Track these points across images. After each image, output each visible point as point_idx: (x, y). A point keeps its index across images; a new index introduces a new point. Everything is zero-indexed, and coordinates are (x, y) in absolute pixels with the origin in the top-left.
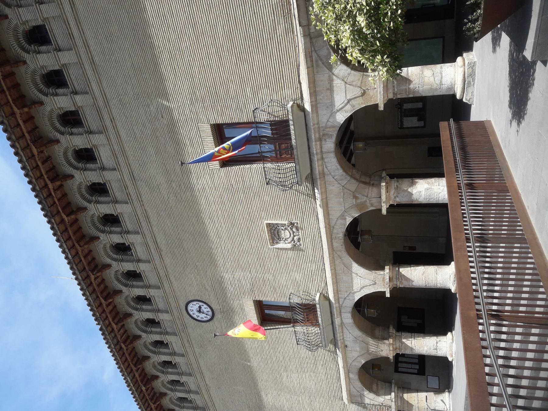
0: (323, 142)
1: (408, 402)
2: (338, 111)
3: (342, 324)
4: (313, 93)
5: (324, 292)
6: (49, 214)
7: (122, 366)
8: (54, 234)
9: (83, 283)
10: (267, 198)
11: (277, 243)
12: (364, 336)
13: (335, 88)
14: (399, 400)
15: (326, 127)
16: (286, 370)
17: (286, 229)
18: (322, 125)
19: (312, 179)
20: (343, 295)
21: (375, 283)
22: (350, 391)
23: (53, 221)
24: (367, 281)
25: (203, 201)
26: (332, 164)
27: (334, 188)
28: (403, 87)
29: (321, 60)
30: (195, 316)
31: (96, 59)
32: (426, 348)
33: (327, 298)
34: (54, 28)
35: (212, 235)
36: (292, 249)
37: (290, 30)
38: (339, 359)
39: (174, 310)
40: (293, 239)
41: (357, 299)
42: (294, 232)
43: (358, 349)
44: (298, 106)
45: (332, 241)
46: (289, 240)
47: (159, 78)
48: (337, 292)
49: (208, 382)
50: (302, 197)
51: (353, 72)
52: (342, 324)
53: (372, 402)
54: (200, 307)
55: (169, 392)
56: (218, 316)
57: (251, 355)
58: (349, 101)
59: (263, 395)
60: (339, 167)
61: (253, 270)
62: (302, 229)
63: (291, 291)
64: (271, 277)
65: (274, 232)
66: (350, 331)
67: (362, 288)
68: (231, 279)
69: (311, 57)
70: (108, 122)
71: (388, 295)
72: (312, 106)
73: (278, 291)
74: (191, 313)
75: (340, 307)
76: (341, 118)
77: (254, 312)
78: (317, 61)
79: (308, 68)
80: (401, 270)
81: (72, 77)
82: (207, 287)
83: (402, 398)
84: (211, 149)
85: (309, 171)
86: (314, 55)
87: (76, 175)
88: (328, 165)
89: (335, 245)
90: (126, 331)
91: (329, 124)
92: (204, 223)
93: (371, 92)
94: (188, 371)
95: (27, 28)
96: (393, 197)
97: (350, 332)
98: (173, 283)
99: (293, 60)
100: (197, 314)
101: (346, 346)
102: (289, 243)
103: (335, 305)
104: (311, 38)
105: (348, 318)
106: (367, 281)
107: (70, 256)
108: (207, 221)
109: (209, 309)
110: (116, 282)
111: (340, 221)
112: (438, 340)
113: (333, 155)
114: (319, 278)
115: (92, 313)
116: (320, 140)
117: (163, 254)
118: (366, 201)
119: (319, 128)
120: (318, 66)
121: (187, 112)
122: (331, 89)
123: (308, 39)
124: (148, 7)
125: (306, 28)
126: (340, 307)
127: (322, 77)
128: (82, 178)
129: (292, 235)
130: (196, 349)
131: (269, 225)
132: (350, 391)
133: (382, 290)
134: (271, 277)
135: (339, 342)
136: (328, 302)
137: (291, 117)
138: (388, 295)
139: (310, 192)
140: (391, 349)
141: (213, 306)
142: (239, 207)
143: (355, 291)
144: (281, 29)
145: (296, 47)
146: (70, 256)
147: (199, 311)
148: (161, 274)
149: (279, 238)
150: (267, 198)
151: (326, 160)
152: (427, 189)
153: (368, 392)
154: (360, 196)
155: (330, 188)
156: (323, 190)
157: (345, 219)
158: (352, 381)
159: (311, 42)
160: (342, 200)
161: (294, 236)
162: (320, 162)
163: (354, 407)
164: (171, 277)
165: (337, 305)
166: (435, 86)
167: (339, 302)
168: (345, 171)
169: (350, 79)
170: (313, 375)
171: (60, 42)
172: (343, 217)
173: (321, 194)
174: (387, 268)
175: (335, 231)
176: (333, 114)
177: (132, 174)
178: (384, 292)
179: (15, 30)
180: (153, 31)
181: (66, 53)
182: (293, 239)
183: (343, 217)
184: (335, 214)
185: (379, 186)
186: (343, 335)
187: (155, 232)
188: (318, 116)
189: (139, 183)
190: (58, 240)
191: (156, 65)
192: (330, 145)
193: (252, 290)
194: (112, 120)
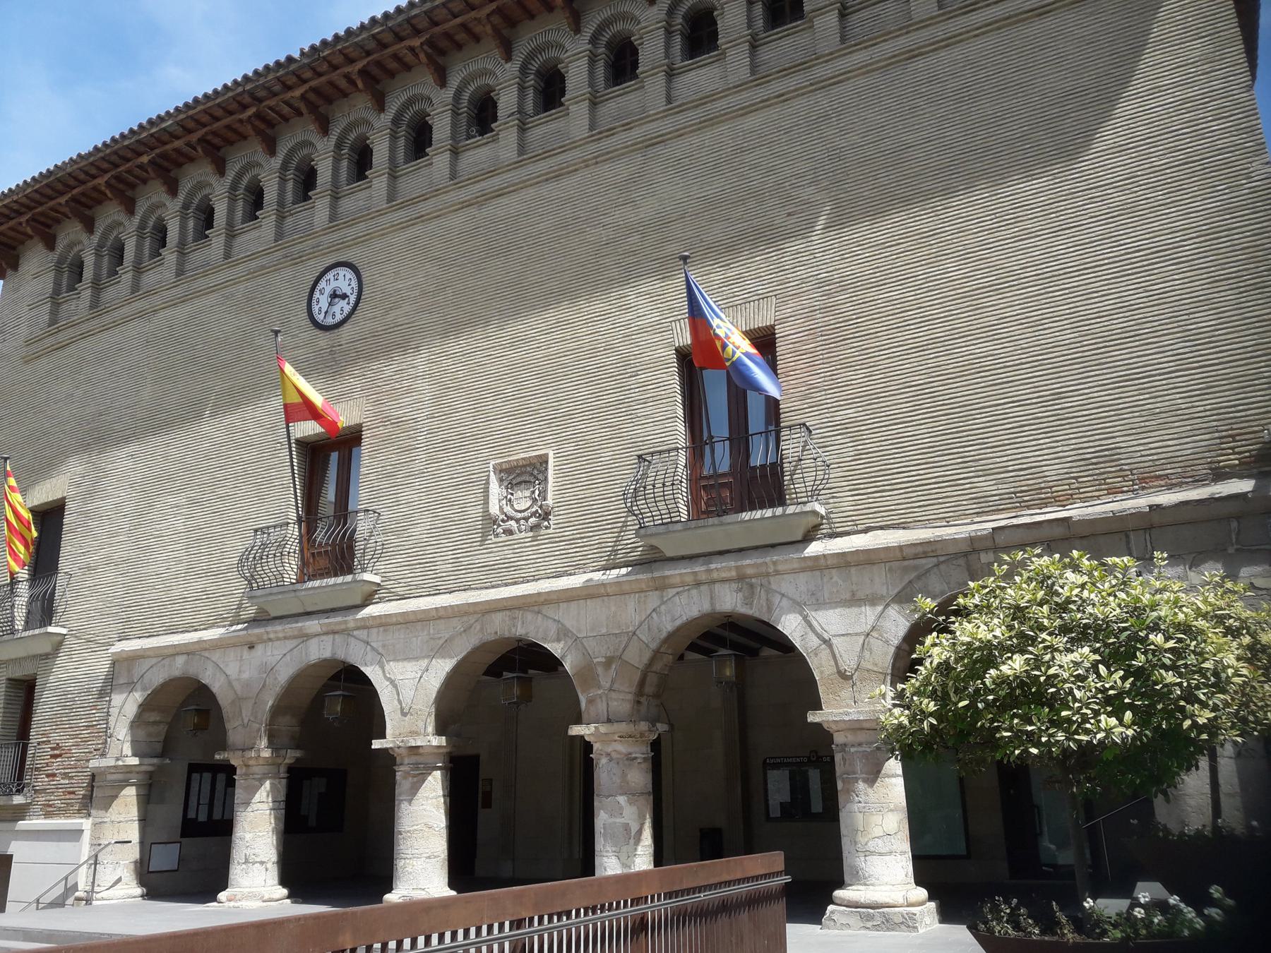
0: (734, 586)
2: (805, 618)
3: (305, 637)
4: (845, 561)
7: (200, 108)
9: (400, 19)
10: (606, 455)
11: (501, 480)
13: (855, 610)
14: (120, 777)
15: (769, 591)
16: (193, 502)
17: (535, 500)
20: (376, 638)
21: (404, 714)
22: (143, 657)
24: (409, 695)
26: (686, 605)
27: (631, 613)
29: (919, 578)
30: (322, 284)
31: (920, 64)
32: (248, 836)
33: (367, 601)
35: (517, 328)
37: (985, 507)
38: (222, 630)
40: (510, 518)
42: (526, 519)
43: (245, 676)
44: (816, 527)
46: (508, 509)
47: (876, 208)
48: (384, 623)
49: (161, 314)
50: (609, 538)
51: (892, 650)
52: (305, 637)
54: (344, 296)
55: (136, 220)
56: (324, 339)
57: (228, 420)
58: (827, 642)
59: (132, 448)
62: (534, 539)
63: (386, 515)
64: (417, 466)
65: (525, 474)
67: (392, 682)
69: (925, 555)
70: (777, 87)
71: (376, 744)
74: (330, 275)
75: (346, 632)
76: (790, 625)
78: (916, 568)
79: (900, 548)
80: (438, 774)
82: (393, 314)
83: (125, 784)
87: (655, 9)
88: (684, 599)
89: (498, 618)
93: (846, 693)
94: (188, 267)
96: (609, 750)
99: (918, 513)
100: (328, 290)
101: (251, 647)
102: (501, 508)
105: (320, 650)
106: (409, 695)
109: (339, 317)
111: (553, 629)
112: (269, 865)
113: (706, 607)
115: (330, 39)
116: (741, 578)
117: (473, 210)
119: (768, 575)
120: (906, 570)
121: (802, 272)
122: (854, 601)
123: (965, 548)
124: (1036, 184)
125: (989, 544)
126: (346, 632)
127: (879, 581)
129: (519, 515)
130: (242, 287)
131: (544, 460)
132: (143, 657)
133: (389, 731)
134: (417, 466)
136: (358, 602)
138: (376, 744)
141: (347, 326)
142: (584, 392)
143: (387, 667)
144: (986, 486)
148: (421, 205)
149: (512, 486)
150: (606, 455)
151: (694, 592)
153: (140, 700)
154: (612, 672)
155: (631, 602)
156: (626, 588)
157: (558, 640)
158: (166, 662)
159: (956, 556)
160: (604, 631)
161: (517, 521)
162: (689, 579)
165: (351, 625)
166: (861, 839)
167: (358, 628)
168: (671, 636)
169: (875, 643)
173: (617, 583)
174: (442, 741)
175: (529, 616)
176: (798, 606)
177: (660, 140)
180: (982, 195)
182: (510, 518)
184: (571, 617)
186: (278, 639)
187: (524, 192)
188: (794, 571)
191: (906, 201)
192: (730, 601)
193: (386, 420)
194: (782, 98)
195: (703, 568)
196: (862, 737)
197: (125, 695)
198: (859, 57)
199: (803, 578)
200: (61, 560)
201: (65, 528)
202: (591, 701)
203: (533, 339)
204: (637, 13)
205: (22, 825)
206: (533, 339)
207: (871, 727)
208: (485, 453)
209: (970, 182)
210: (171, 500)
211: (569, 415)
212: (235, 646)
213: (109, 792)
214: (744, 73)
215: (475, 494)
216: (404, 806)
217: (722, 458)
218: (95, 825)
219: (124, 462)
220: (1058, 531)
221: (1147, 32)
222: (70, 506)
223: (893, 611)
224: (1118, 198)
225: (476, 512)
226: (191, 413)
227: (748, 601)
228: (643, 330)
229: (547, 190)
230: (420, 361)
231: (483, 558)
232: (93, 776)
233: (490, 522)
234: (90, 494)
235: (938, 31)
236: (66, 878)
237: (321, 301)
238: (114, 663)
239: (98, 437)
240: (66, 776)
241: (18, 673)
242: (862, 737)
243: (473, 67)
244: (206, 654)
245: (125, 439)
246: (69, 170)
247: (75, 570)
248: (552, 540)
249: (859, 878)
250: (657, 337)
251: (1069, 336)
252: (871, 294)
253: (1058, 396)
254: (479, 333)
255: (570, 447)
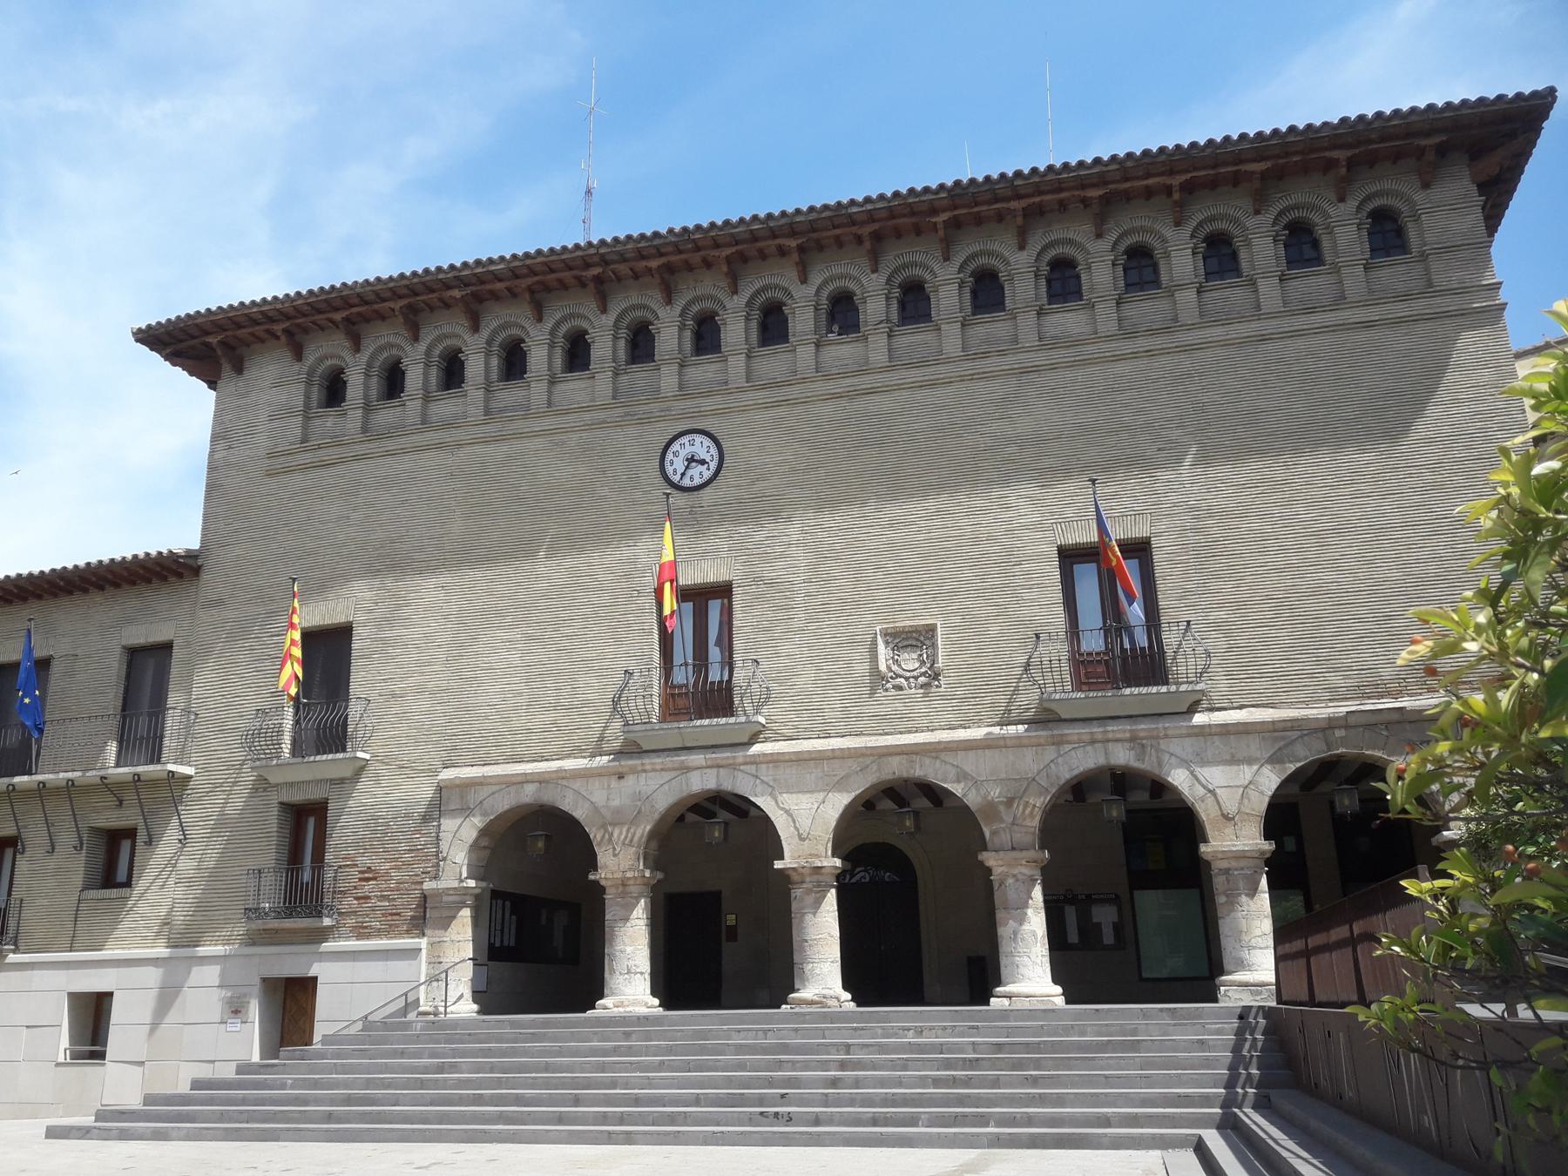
0: (1127, 745)
1: (454, 917)
2: (1192, 773)
3: (686, 769)
4: (1226, 730)
5: (768, 734)
6: (958, 191)
7: (540, 259)
8: (912, 191)
9: (783, 221)
10: (994, 630)
11: (887, 643)
12: (656, 816)
13: (1235, 768)
14: (456, 898)
15: (1158, 750)
16: (530, 638)
17: (923, 663)
18: (1163, 744)
19: (631, 750)
20: (766, 773)
21: (801, 839)
22: (481, 784)
23: (944, 195)
24: (806, 825)
25: (979, 503)
26: (1083, 759)
27: (1029, 763)
28: (1241, 884)
29: (1286, 746)
31: (1269, 346)
32: (629, 949)
33: (753, 739)
34: (1313, 280)
35: (893, 511)
36: (875, 672)
37: (1336, 696)
38: (586, 761)
39: (689, 403)
40: (898, 676)
41: (759, 801)
42: (916, 678)
43: (616, 803)
44: (1198, 702)
45: (902, 753)
46: (895, 668)
47: (1238, 452)
48: (775, 760)
49: (468, 449)
50: (1002, 700)
51: (1267, 800)
52: (686, 769)
53: (446, 837)
54: (703, 462)
55: (422, 347)
56: (678, 500)
57: (569, 562)
58: (1213, 792)
59: (445, 579)
60: (1076, 772)
61: (813, 588)
62: (925, 695)
63: (764, 665)
64: (796, 624)
65: (917, 639)
66: (666, 787)
67: (787, 812)
68: (785, 539)
69: (1292, 729)
70: (1142, 343)
71: (778, 865)
72: (1202, 727)
73: (761, 637)
75: (733, 766)
76: (1179, 778)
77: (699, 581)
78: (1283, 738)
79: (1273, 722)
80: (833, 891)
81: (1227, 292)
82: (760, 485)
83: (463, 905)
84: (1117, 532)
85: (645, 748)
86: (1296, 734)
87: (1025, 253)
88: (1080, 752)
89: (895, 760)
90: (619, 279)
91: (1167, 757)
92: (925, 497)
93: (1229, 830)
94: (493, 405)
95: (1319, 231)
96: (1016, 872)
97: (661, 788)
98: (764, 408)
99: (1283, 697)
100: (683, 453)
101: (621, 777)
102: (889, 668)
103: (740, 755)
104: (1324, 730)
105: (702, 781)
106: (806, 825)
107: (855, 209)
108: (931, 504)
109: (697, 481)
110: (757, 285)
111: (952, 772)
113: (1102, 761)
114: (806, 725)
115: (705, 225)
116: (1133, 739)
117: (843, 402)
118: (1002, 821)
119: (1158, 737)
120: (1276, 739)
121: (1173, 498)
122: (1234, 761)
123: (1324, 725)
124: (1367, 457)
125: (1343, 723)
126: (733, 766)
127: (1254, 746)
128: (1022, 270)
130: (575, 436)
131: (932, 629)
132: (481, 784)
133: (786, 854)
134: (796, 624)
135: (638, 762)
136: (745, 740)
137: (1173, 688)
139: (606, 747)
140: (629, 875)
141: (707, 490)
142: (968, 574)
143: (780, 798)
144: (1336, 679)
145: (1306, 704)
146: (855, 209)
147: (691, 460)
148: (787, 389)
149: (897, 648)
150: (994, 630)
151: (1089, 748)
152: (1035, 935)
153: (481, 825)
155: (1029, 754)
156: (1026, 741)
157: (958, 781)
158: (512, 789)
159: (1316, 730)
160: (1003, 776)
161: (907, 679)
162: (1087, 738)
163: (426, 792)
164: (782, 409)
165: (741, 760)
166: (1245, 938)
167: (745, 764)
168: (1068, 782)
169: (1252, 793)
170: (523, 700)
171: (1294, 283)
172: (962, 776)
173: (1018, 737)
174: (838, 862)
175: (927, 761)
176: (1185, 763)
177: (1036, 369)
178: (782, 858)
179: (1313, 207)
180: (1324, 457)
181: (1277, 293)
182: (898, 676)
183: (962, 776)
184: (968, 762)
185: (1042, 848)
186: (654, 770)
187: (897, 393)
188: (1180, 736)
189: (1014, 381)
190: (896, 194)
191: (1262, 453)
193: (757, 580)
194: (1150, 354)
195: (110, 771)
196: (1243, 863)
197: (459, 821)
198: (1217, 332)
199: (1188, 741)
200: (352, 686)
201: (354, 653)
202: (994, 833)
203: (912, 523)
204: (1006, 254)
205: (327, 946)
206: (912, 523)
207: (1240, 856)
208: (869, 618)
209: (1316, 444)
210: (501, 634)
211: (954, 592)
212: (600, 775)
213: (446, 913)
214: (1112, 327)
215: (862, 653)
216: (809, 917)
217: (1093, 642)
218: (432, 944)
219: (431, 595)
220: (1395, 716)
221: (1449, 356)
222: (358, 632)
223: (1266, 770)
224: (1429, 477)
225: (862, 668)
226: (522, 549)
227: (1140, 758)
228: (1025, 527)
229: (920, 395)
230: (794, 531)
231: (872, 708)
232: (424, 897)
233: (878, 679)
234: (389, 621)
235: (1286, 324)
236: (406, 994)
237: (675, 465)
238: (440, 789)
239: (392, 561)
240: (384, 898)
241: (298, 797)
242: (1243, 863)
243: (836, 270)
244: (564, 782)
245: (428, 568)
246: (358, 290)
247: (373, 696)
248: (943, 698)
249: (1241, 965)
250: (1039, 535)
251: (1397, 575)
252: (1234, 523)
253: (1390, 618)
254: (856, 512)
255: (957, 620)
